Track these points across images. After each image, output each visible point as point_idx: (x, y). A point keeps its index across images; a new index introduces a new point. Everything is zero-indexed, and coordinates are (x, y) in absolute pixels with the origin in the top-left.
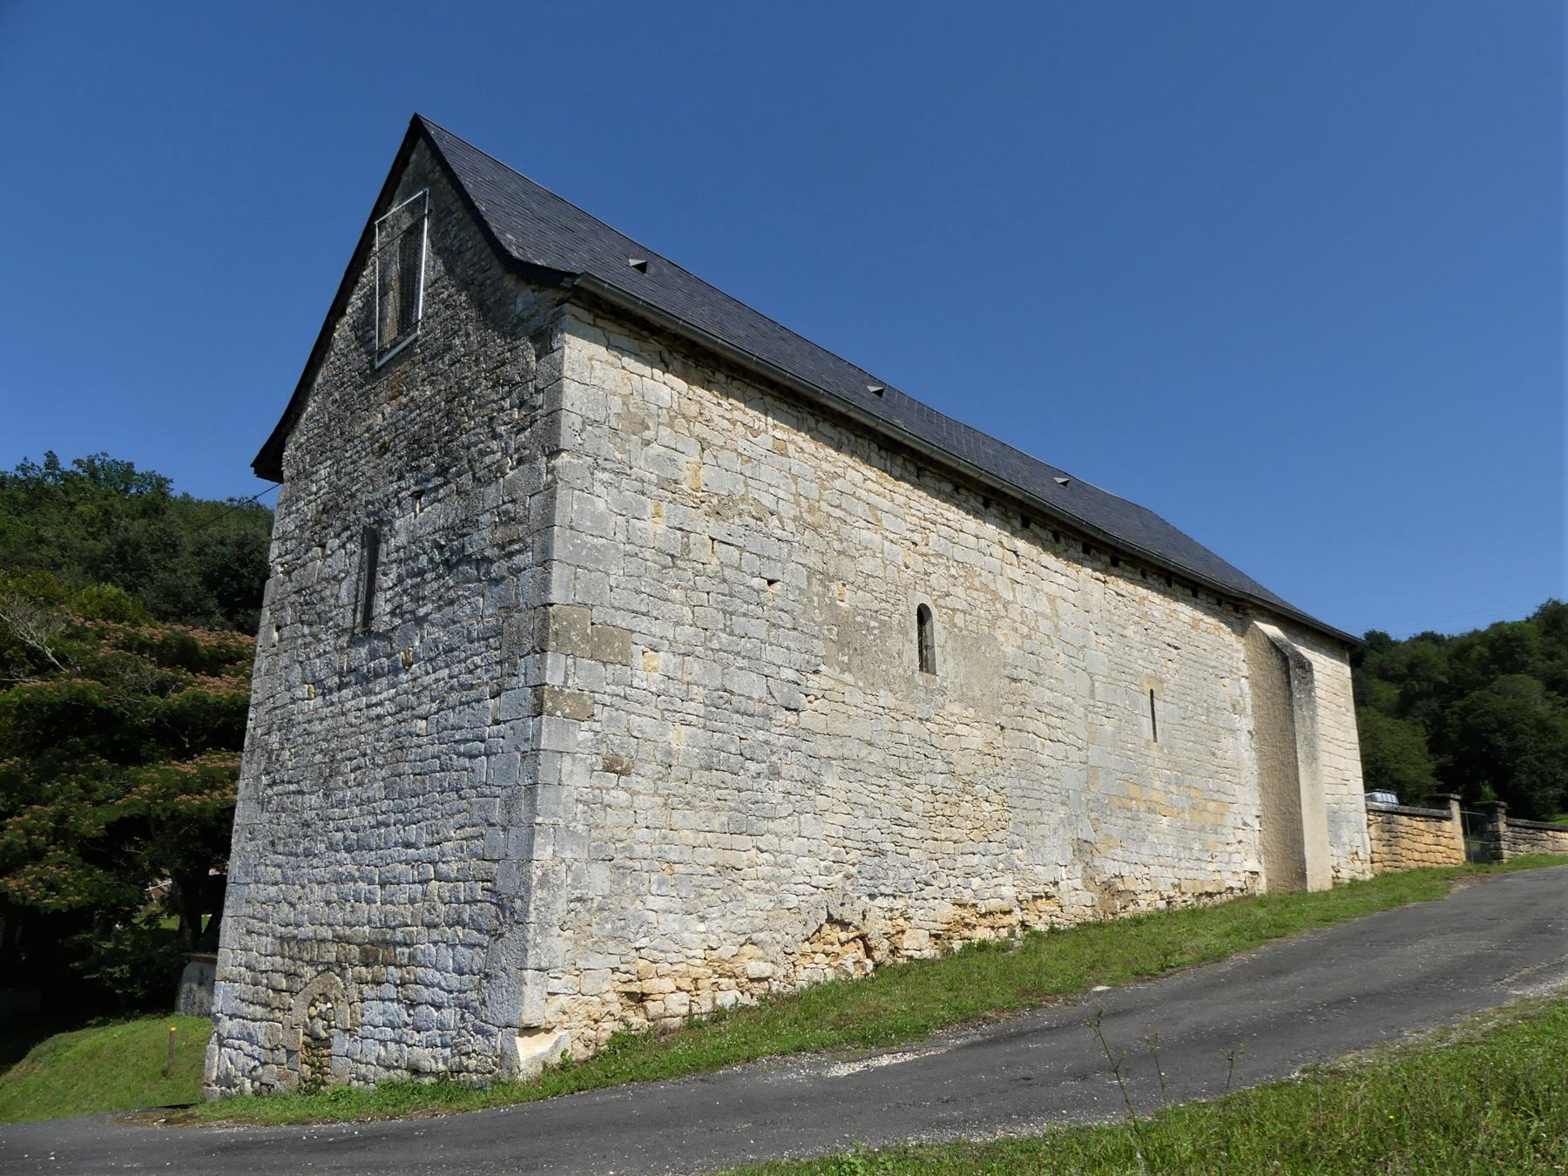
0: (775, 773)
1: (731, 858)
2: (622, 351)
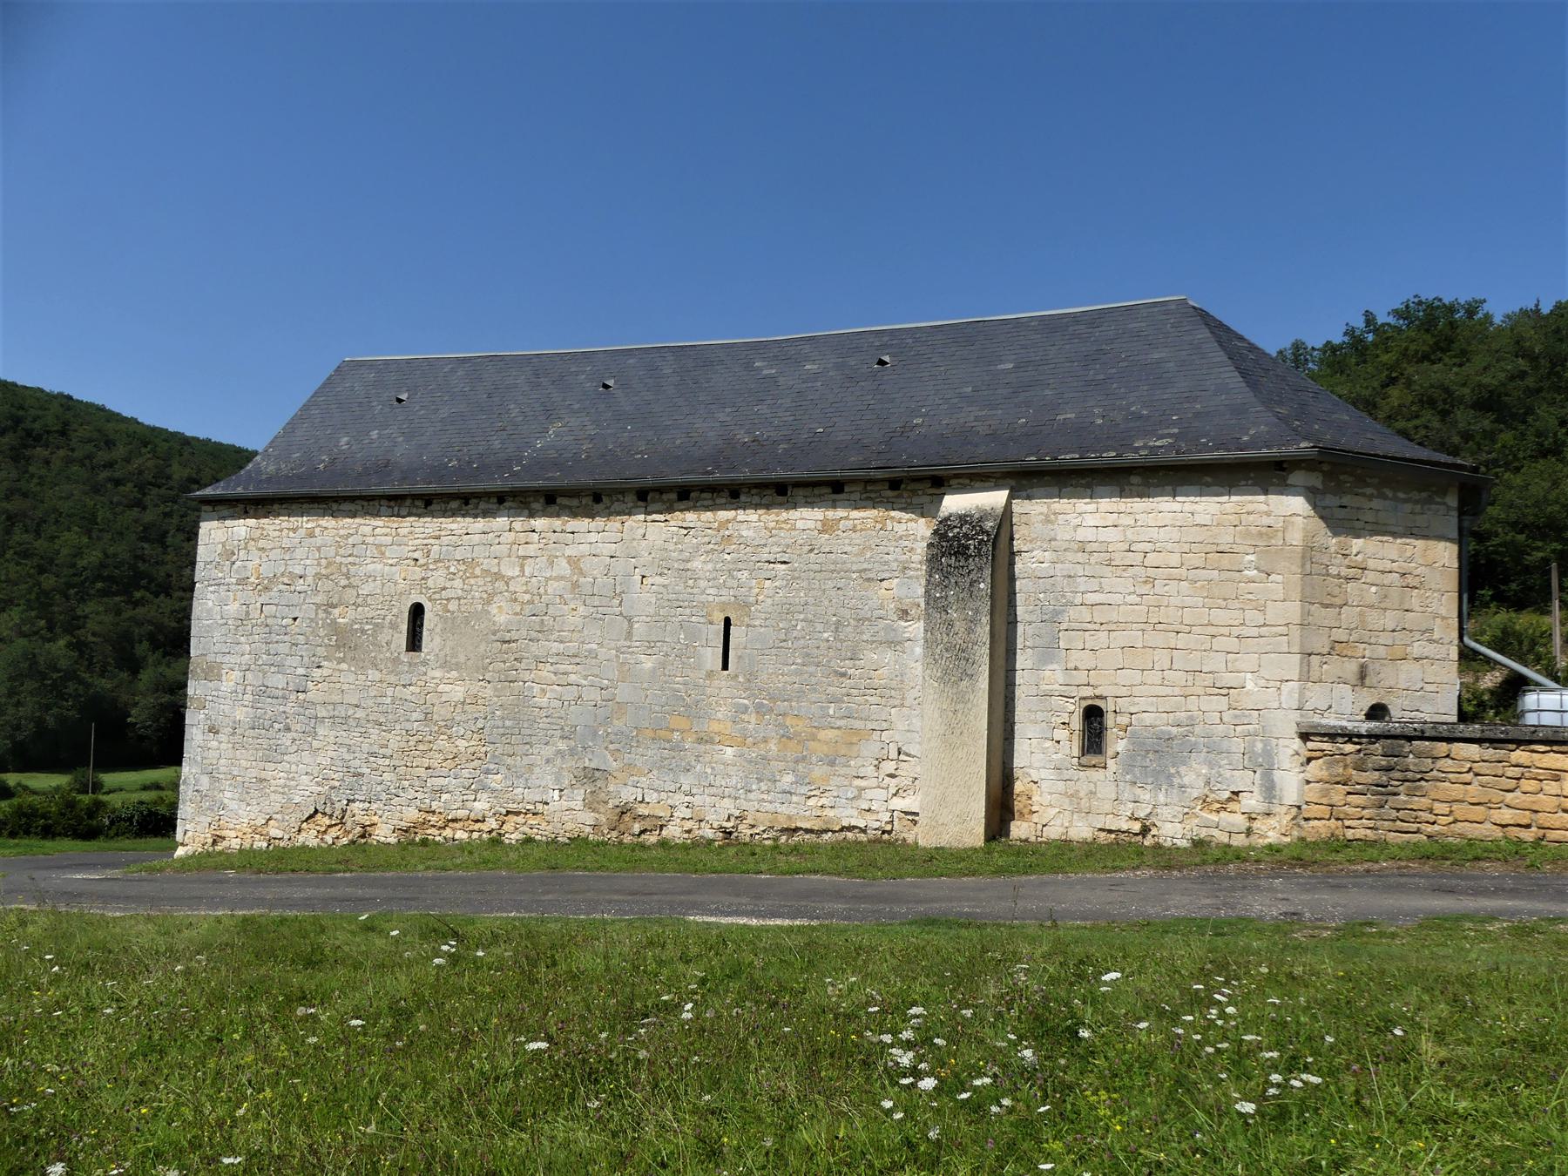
0: (288, 729)
1: (263, 775)
2: (224, 518)
